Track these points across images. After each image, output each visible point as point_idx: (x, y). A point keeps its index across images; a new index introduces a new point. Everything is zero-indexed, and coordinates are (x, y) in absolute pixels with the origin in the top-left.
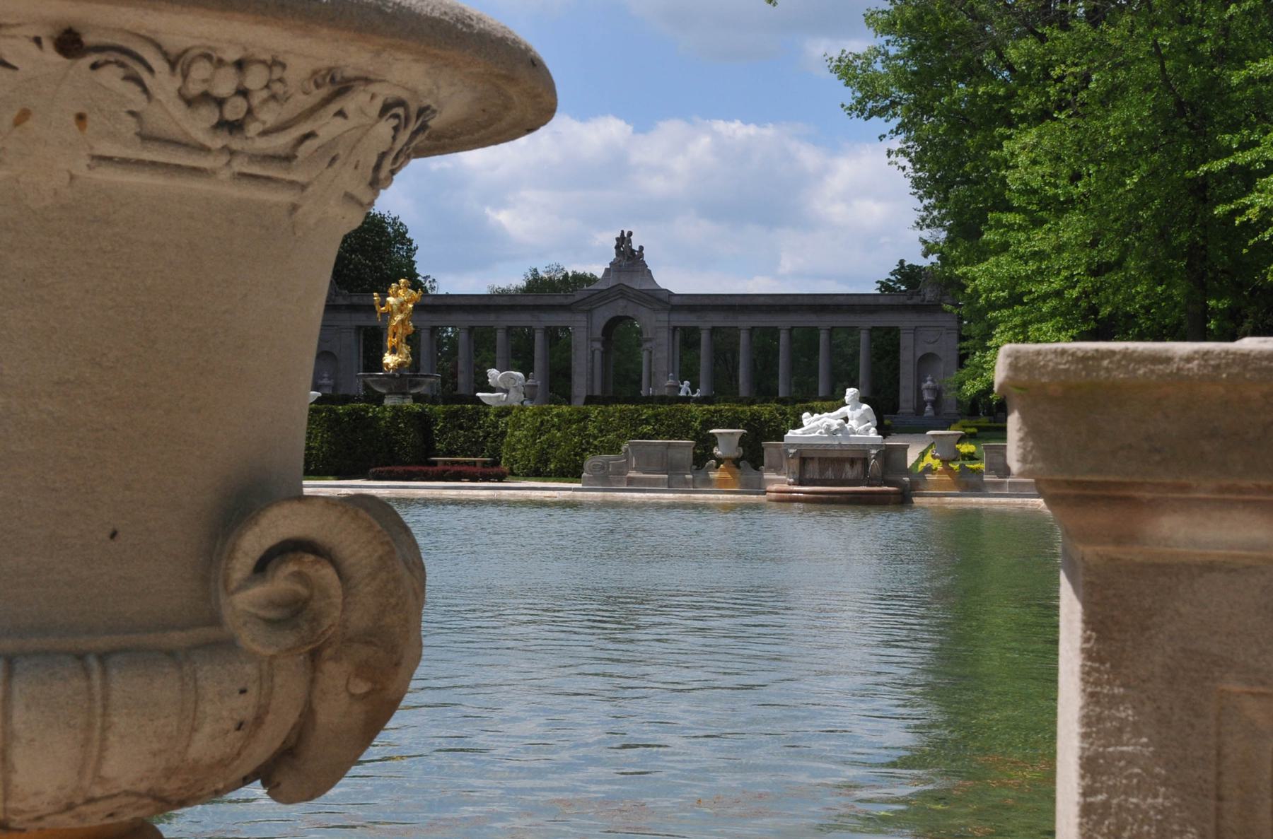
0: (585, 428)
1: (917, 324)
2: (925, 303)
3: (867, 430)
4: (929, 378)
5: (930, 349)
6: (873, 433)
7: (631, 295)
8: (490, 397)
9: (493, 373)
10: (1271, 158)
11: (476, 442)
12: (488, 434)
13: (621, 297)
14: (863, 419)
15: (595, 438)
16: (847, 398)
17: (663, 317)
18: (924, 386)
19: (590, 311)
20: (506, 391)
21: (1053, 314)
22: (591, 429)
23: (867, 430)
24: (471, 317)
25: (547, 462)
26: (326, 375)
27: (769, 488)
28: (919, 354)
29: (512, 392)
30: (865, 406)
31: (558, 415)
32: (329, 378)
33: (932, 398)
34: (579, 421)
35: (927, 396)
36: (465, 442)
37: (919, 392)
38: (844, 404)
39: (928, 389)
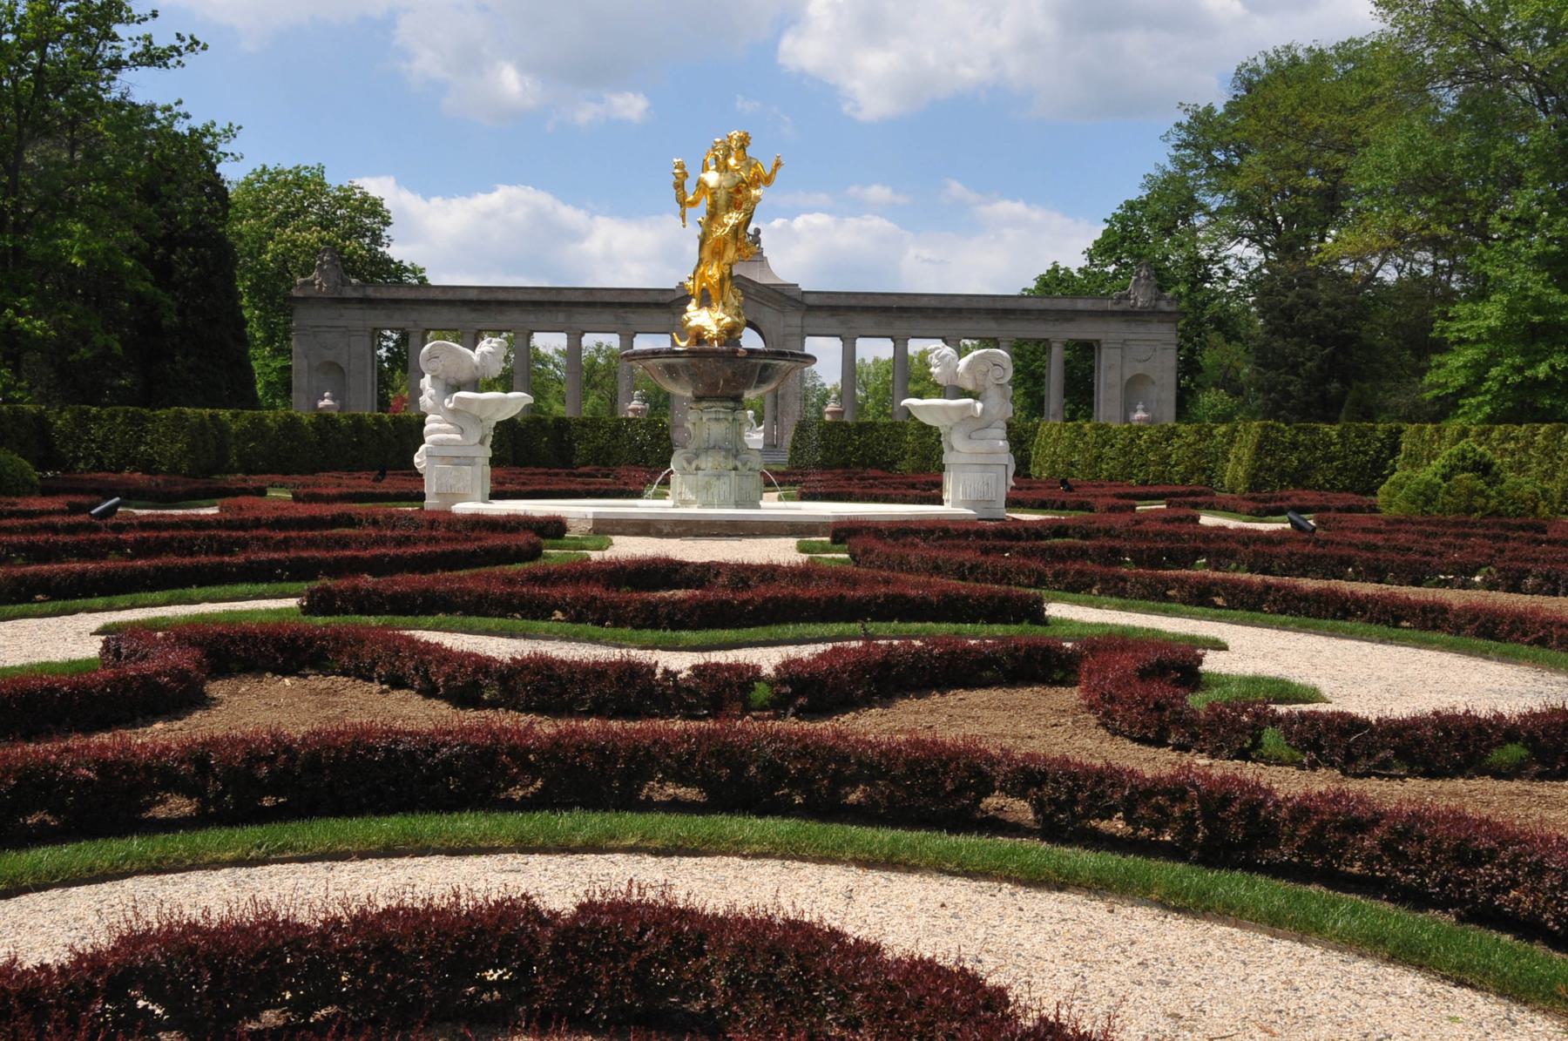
4: (1140, 406)
5: (1140, 369)
8: (944, 408)
26: (327, 394)
28: (1128, 376)
32: (333, 399)
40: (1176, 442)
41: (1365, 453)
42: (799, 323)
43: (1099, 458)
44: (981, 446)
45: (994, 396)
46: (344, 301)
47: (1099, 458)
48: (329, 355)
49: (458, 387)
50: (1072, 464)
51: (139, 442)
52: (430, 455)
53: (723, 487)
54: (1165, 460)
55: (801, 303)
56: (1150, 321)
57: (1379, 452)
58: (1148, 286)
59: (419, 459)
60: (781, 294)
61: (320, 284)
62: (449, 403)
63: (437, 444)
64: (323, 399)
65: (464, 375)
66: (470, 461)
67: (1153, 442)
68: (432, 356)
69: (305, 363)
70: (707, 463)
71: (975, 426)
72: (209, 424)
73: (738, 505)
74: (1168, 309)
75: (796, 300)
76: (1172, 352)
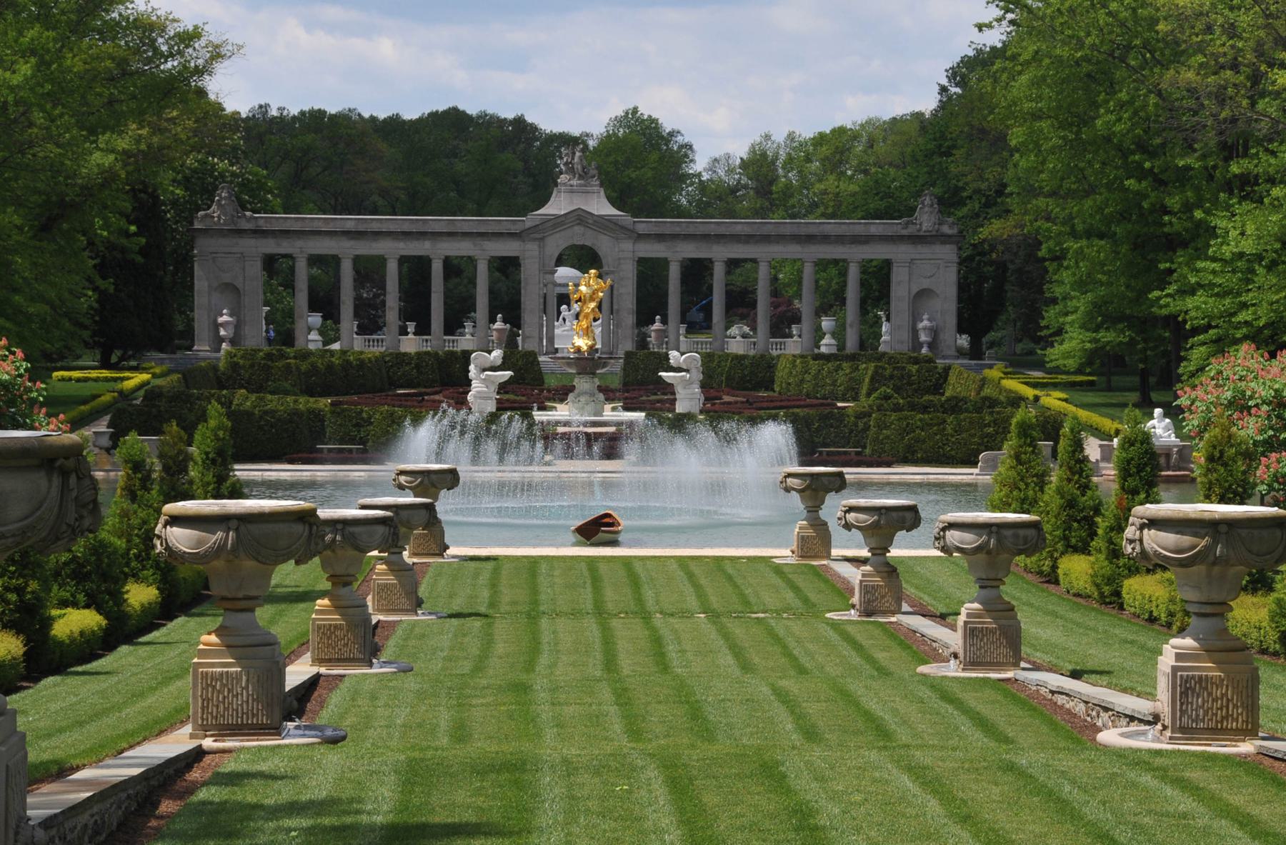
0: (944, 429)
1: (913, 256)
2: (922, 233)
3: (1170, 435)
4: (925, 317)
5: (926, 284)
6: (1173, 438)
7: (590, 221)
8: (674, 377)
9: (674, 354)
10: (1284, 35)
11: (844, 437)
12: (851, 431)
13: (579, 224)
14: (1166, 429)
15: (952, 436)
16: (1155, 415)
17: (627, 246)
18: (921, 325)
19: (542, 239)
20: (687, 371)
21: (1245, 338)
22: (949, 430)
23: (1170, 435)
24: (402, 245)
25: (914, 452)
26: (225, 311)
27: (1104, 472)
28: (915, 290)
29: (694, 371)
30: (1168, 420)
31: (921, 420)
32: (231, 315)
33: (928, 339)
34: (939, 424)
35: (923, 337)
36: (835, 437)
37: (915, 332)
38: (1153, 418)
39: (925, 329)
40: (841, 373)
41: (931, 381)
42: (562, 623)
43: (802, 381)
44: (689, 391)
45: (694, 371)
46: (240, 232)
47: (802, 381)
48: (227, 278)
49: (484, 370)
50: (789, 384)
51: (268, 380)
52: (475, 397)
53: (589, 408)
54: (834, 383)
55: (632, 231)
56: (934, 243)
57: (937, 380)
58: (931, 213)
59: (470, 397)
60: (616, 224)
61: (219, 217)
62: (483, 376)
63: (478, 392)
64: (222, 315)
65: (488, 365)
66: (490, 398)
67: (829, 372)
68: (476, 358)
69: (206, 284)
70: (583, 399)
71: (688, 383)
72: (294, 369)
73: (595, 415)
74: (950, 232)
75: (629, 230)
76: (953, 270)
